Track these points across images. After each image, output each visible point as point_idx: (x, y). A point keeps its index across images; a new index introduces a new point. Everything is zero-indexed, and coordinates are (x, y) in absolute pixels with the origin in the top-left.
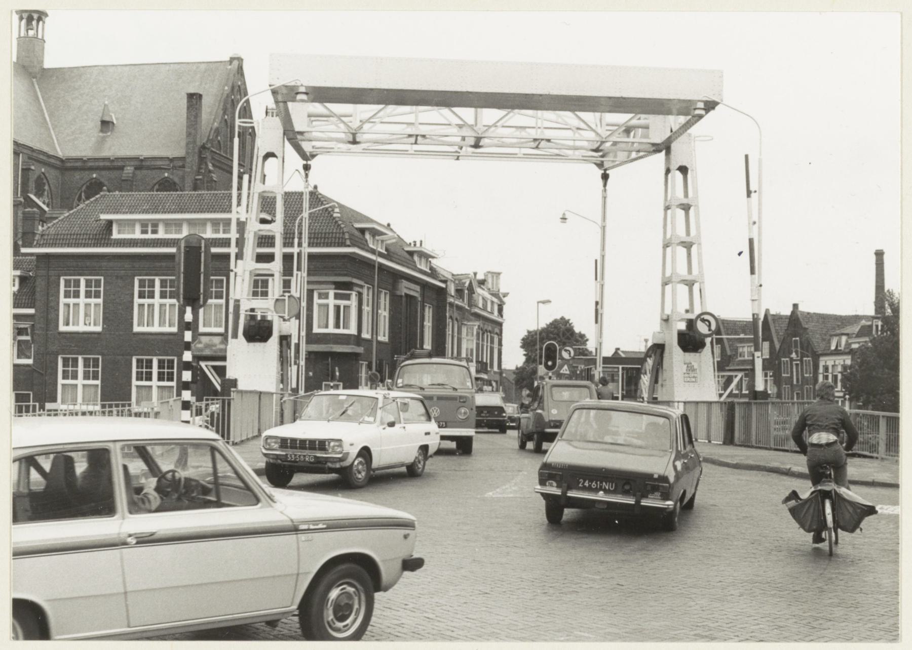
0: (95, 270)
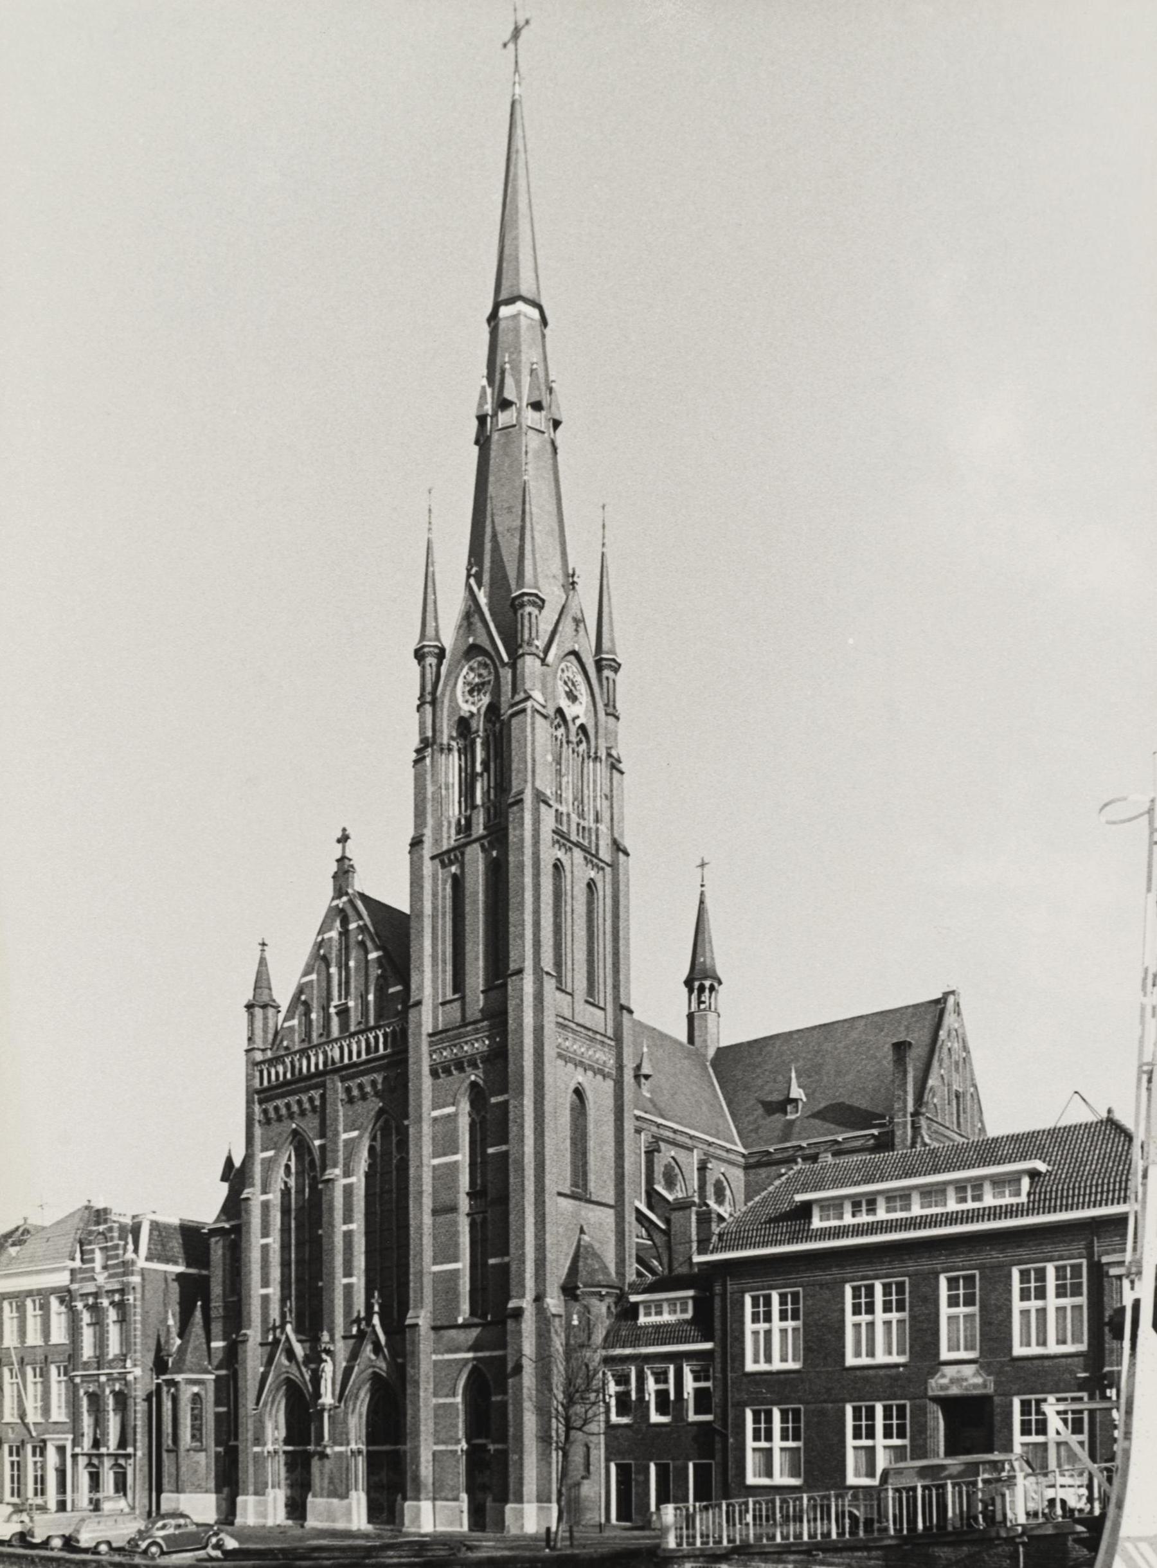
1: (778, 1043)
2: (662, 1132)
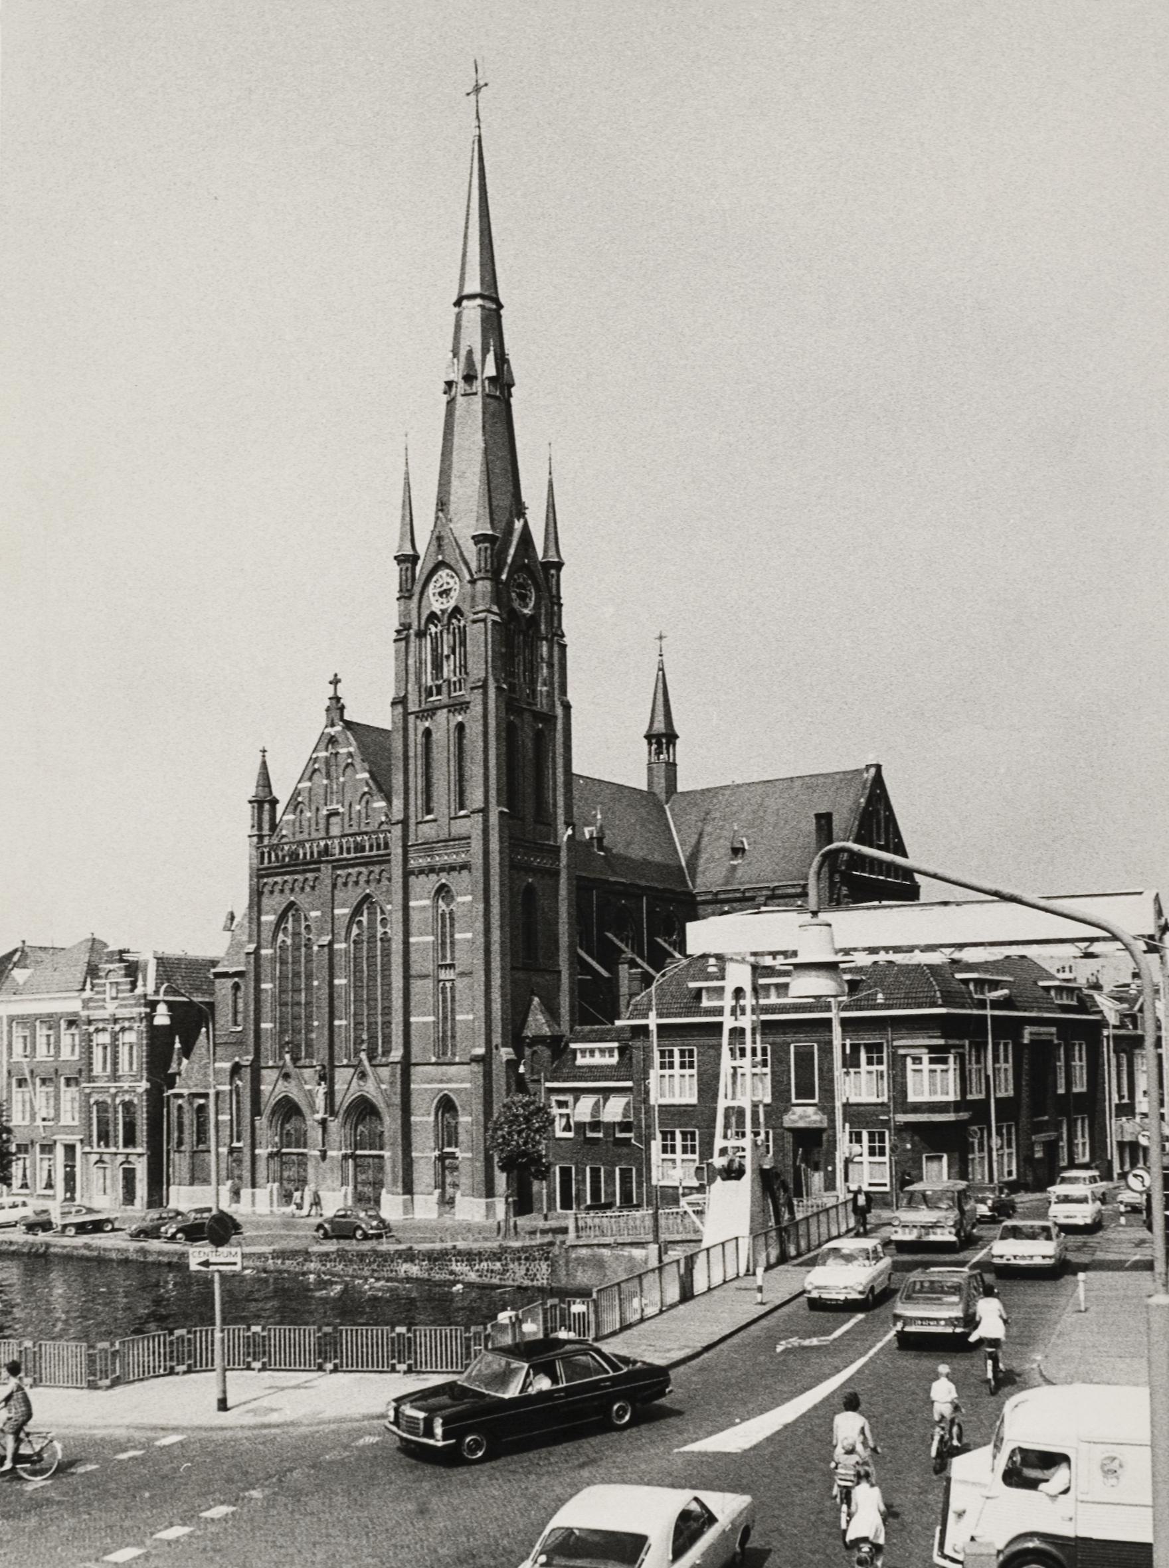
1: (728, 792)
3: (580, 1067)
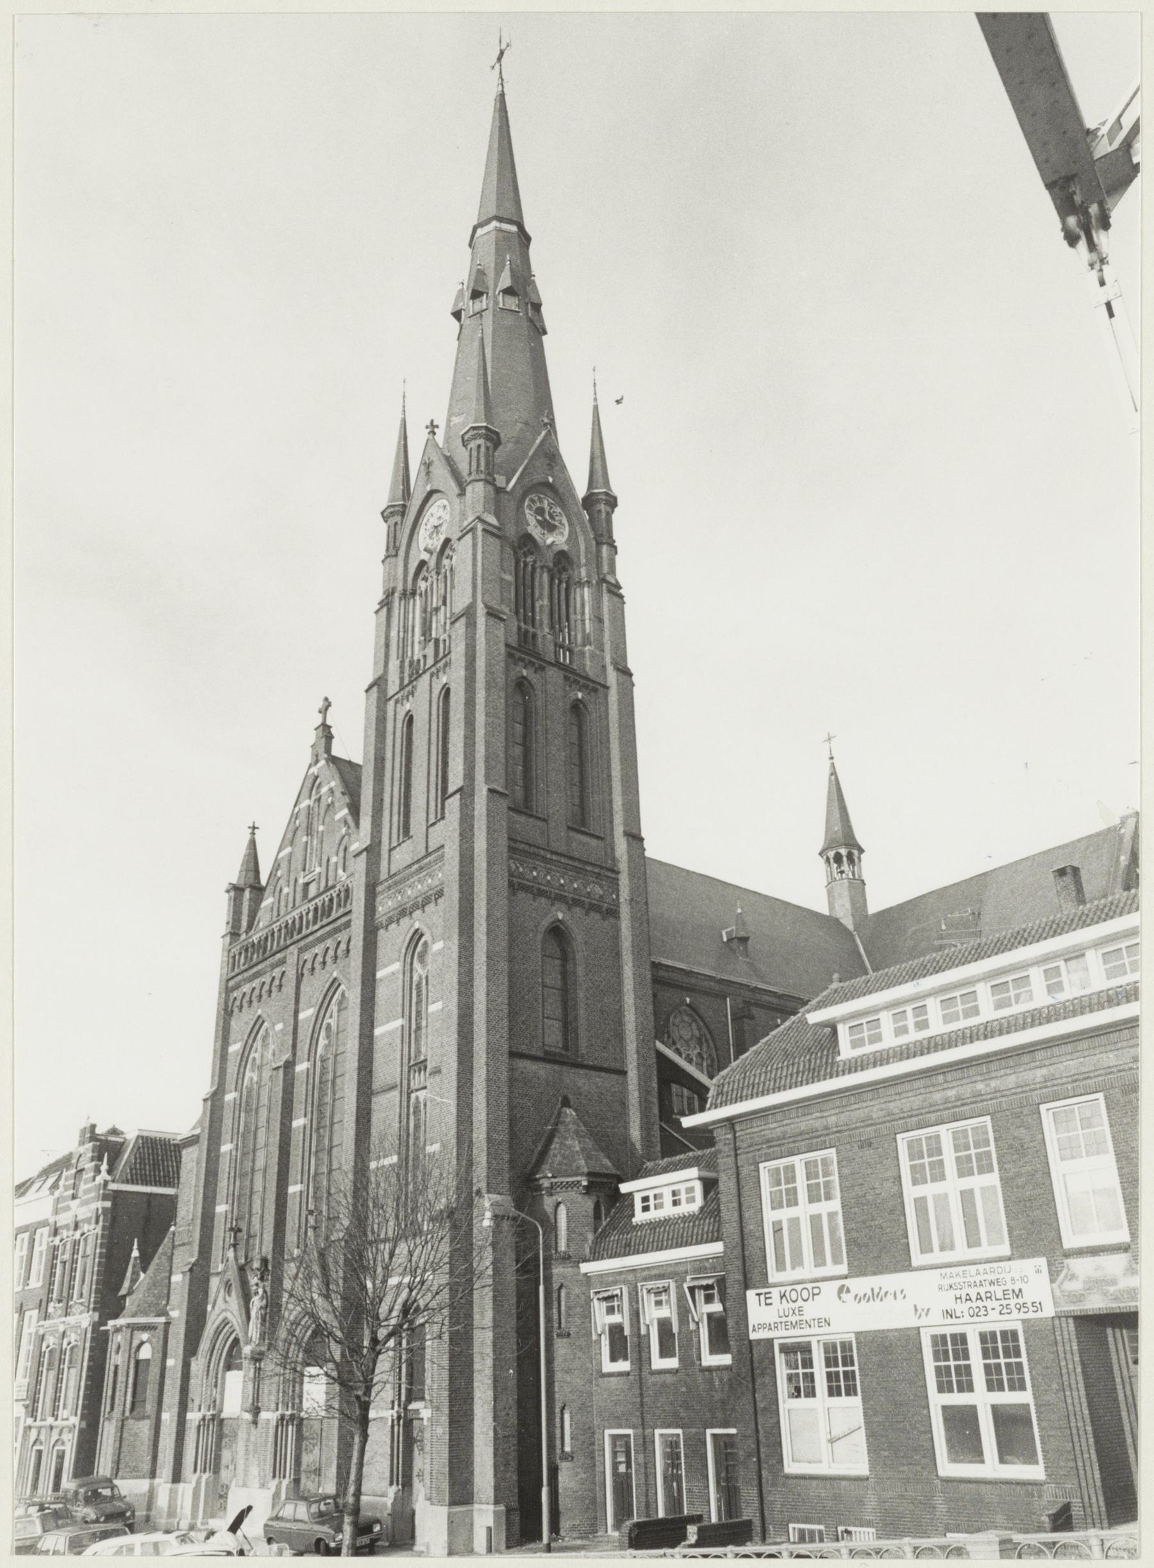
0: (819, 1137)
2: (758, 996)
3: (641, 1226)
